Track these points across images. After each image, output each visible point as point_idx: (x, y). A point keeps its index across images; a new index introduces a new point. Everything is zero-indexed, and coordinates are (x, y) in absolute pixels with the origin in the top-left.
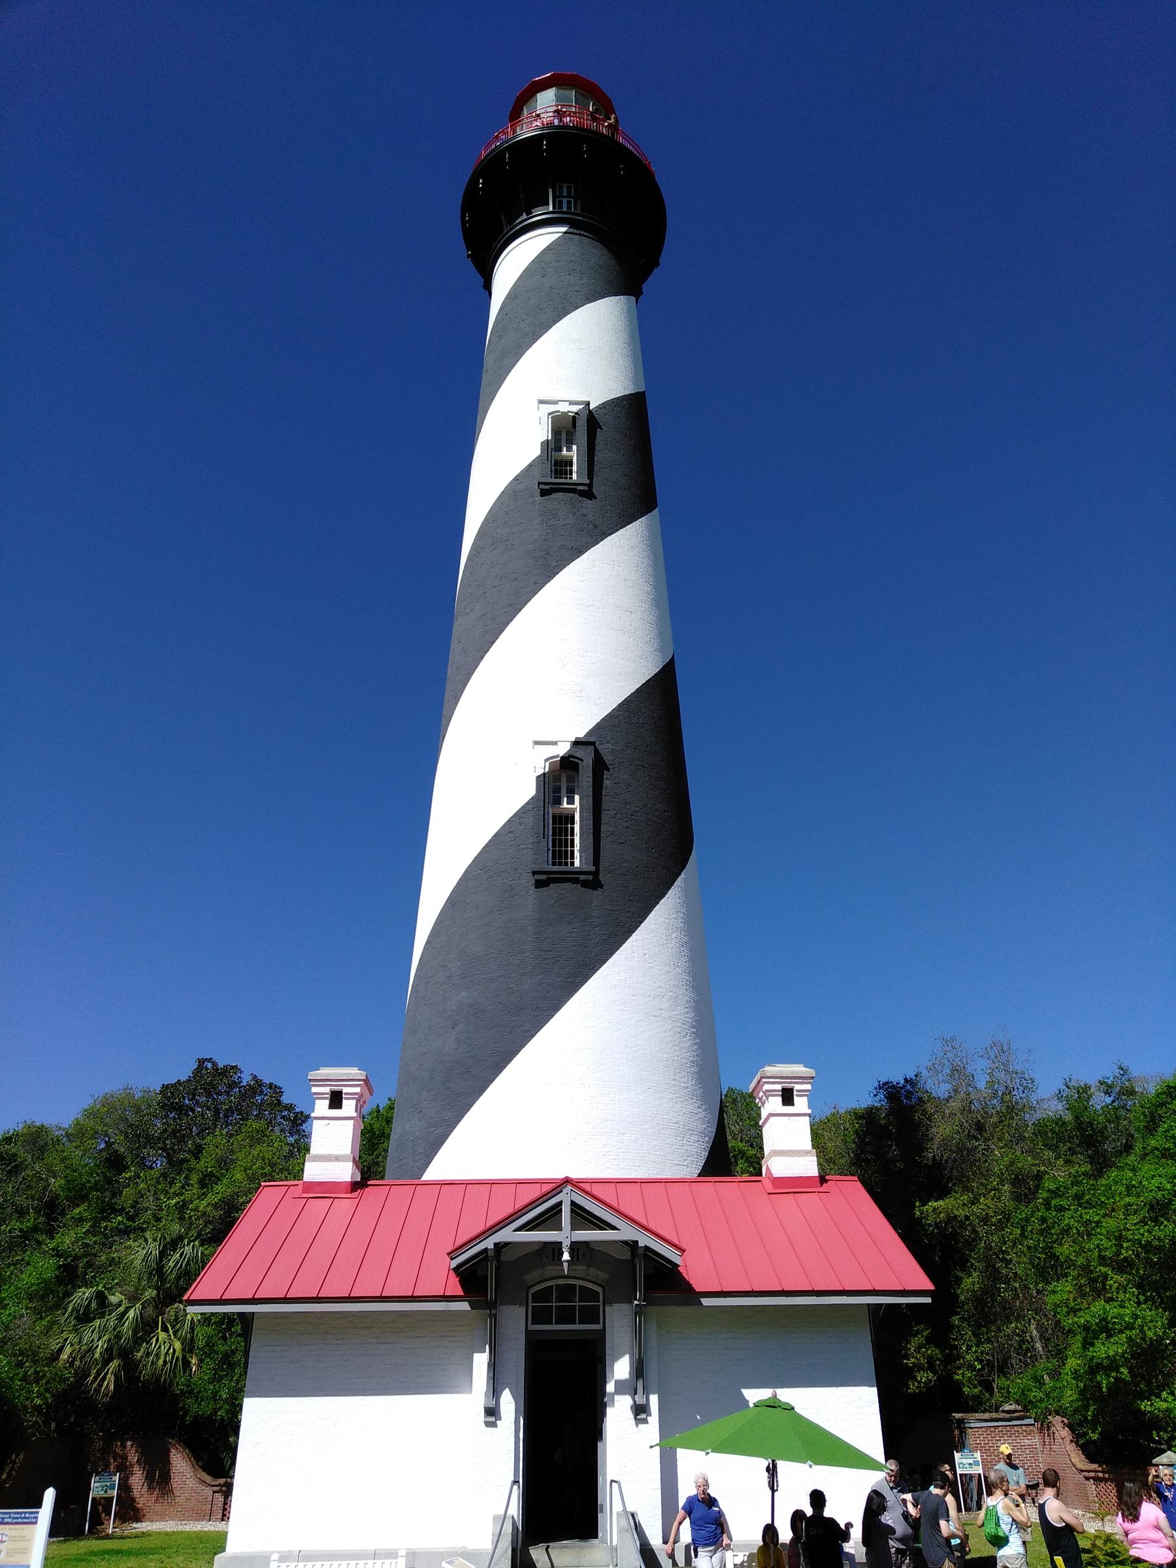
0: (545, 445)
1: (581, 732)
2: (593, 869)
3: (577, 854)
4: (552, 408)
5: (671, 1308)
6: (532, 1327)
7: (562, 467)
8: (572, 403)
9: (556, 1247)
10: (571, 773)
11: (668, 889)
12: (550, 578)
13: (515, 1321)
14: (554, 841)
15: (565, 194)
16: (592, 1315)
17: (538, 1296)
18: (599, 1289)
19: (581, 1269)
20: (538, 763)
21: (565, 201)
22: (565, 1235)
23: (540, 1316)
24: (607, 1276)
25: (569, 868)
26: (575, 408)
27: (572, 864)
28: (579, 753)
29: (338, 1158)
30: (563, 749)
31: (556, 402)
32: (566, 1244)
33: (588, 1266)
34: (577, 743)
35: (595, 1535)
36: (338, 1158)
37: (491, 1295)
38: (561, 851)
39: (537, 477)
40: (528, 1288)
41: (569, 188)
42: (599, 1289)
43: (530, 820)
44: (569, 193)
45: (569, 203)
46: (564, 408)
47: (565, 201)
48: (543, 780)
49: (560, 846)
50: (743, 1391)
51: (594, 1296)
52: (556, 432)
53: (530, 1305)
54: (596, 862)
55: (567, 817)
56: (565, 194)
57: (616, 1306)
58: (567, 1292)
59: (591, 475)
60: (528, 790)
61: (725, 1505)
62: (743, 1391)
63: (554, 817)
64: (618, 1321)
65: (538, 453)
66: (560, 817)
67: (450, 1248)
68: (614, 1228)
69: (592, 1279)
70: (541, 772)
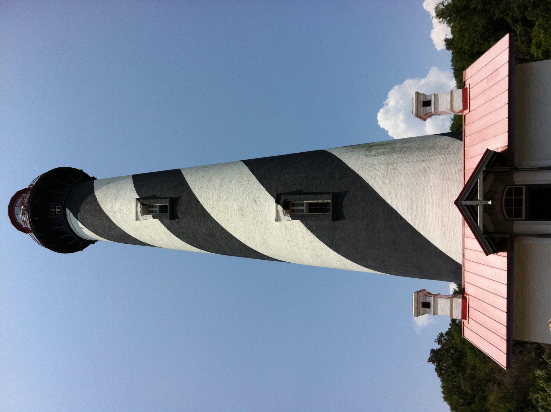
0: (154, 217)
1: (273, 200)
2: (331, 194)
3: (325, 202)
4: (139, 214)
7: (163, 209)
8: (137, 206)
9: (486, 208)
10: (291, 204)
11: (341, 160)
12: (209, 215)
13: (521, 226)
14: (320, 212)
16: (519, 190)
17: (510, 215)
18: (507, 187)
20: (286, 220)
21: (57, 210)
22: (479, 202)
23: (518, 214)
25: (331, 205)
26: (139, 205)
27: (329, 203)
28: (282, 200)
29: (451, 305)
30: (280, 208)
31: (137, 213)
32: (484, 203)
34: (278, 202)
36: (451, 305)
37: (507, 236)
38: (322, 208)
39: (167, 221)
40: (506, 220)
42: (507, 187)
45: (58, 208)
46: (139, 209)
47: (57, 210)
48: (293, 218)
49: (315, 206)
51: (510, 190)
52: (150, 212)
53: (514, 219)
54: (329, 193)
55: (309, 206)
58: (508, 203)
59: (166, 198)
60: (298, 224)
61: (26, 179)
63: (309, 212)
64: (523, 179)
65: (298, 221)
68: (477, 183)
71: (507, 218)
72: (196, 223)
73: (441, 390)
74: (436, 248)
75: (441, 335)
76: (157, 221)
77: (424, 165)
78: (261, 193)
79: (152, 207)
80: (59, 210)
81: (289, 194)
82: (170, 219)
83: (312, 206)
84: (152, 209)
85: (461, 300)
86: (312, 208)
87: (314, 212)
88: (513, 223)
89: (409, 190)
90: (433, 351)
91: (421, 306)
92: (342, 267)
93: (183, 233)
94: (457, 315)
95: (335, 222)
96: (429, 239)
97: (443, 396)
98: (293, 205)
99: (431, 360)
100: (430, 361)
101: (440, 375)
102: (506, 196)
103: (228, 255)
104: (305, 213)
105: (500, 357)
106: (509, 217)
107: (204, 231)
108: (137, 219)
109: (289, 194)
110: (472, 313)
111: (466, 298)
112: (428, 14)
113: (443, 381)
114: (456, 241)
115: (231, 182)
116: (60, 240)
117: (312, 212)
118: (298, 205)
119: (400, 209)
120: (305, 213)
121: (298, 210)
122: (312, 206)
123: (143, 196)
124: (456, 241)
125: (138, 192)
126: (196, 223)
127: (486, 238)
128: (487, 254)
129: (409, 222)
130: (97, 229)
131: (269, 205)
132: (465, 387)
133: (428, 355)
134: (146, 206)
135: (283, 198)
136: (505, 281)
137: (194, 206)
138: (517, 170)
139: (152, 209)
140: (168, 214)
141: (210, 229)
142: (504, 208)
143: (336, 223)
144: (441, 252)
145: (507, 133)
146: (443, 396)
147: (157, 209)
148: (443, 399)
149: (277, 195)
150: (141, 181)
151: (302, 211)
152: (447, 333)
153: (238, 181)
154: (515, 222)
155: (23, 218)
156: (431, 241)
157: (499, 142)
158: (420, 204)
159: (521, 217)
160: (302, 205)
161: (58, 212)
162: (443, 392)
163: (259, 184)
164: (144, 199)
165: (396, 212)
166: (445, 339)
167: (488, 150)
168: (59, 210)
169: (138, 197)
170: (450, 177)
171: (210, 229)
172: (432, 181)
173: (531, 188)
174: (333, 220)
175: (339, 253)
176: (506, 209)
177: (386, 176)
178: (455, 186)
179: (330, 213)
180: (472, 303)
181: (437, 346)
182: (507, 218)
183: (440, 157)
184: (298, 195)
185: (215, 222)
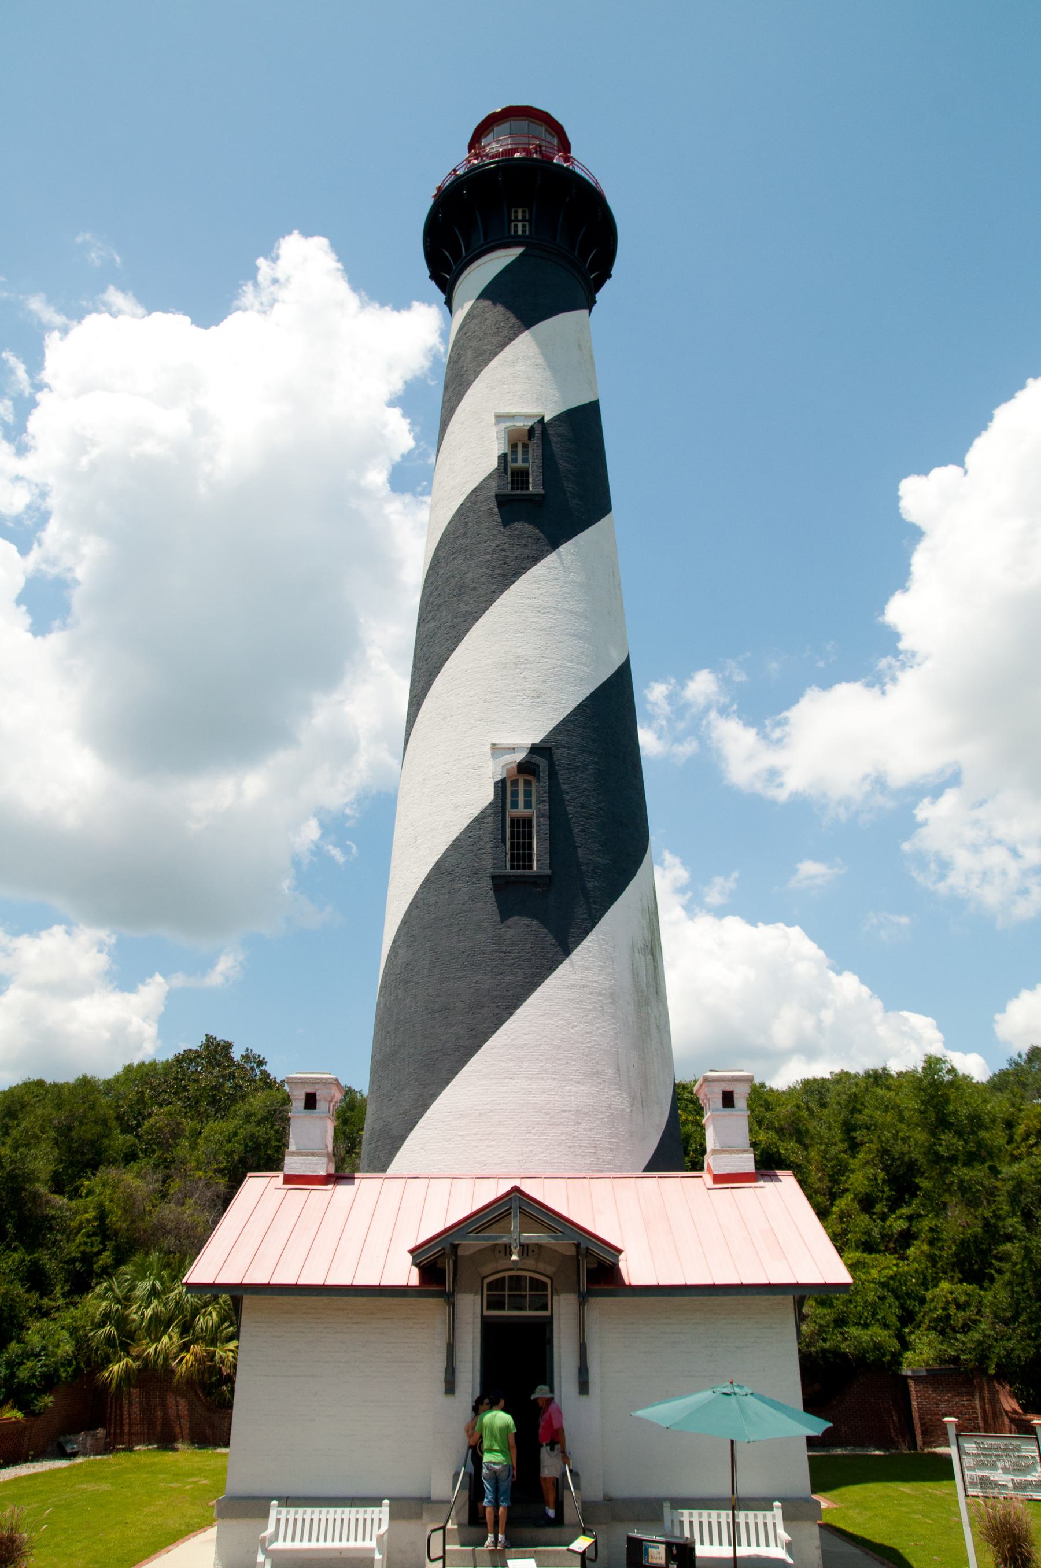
0: (503, 459)
1: (537, 741)
5: (599, 1299)
6: (487, 1313)
8: (527, 417)
12: (507, 586)
13: (471, 1308)
15: (520, 218)
17: (492, 1286)
18: (548, 1281)
19: (530, 1263)
21: (520, 225)
23: (494, 1303)
24: (554, 1269)
25: (527, 872)
30: (520, 756)
33: (537, 1260)
34: (534, 749)
35: (315, 1108)
38: (521, 855)
39: (493, 489)
40: (483, 1279)
41: (524, 212)
42: (548, 1281)
43: (489, 823)
44: (524, 217)
45: (524, 226)
47: (520, 225)
48: (501, 786)
49: (524, 832)
50: (831, 1425)
51: (544, 1286)
52: (514, 446)
55: (524, 820)
56: (520, 218)
57: (562, 1296)
58: (516, 1282)
60: (486, 795)
61: (591, 157)
62: (831, 1425)
63: (512, 821)
64: (563, 1309)
65: (492, 797)
66: (518, 821)
67: (442, 1386)
69: (542, 1270)
70: (499, 778)
71: (487, 1281)
72: (489, 557)
73: (213, 328)
74: (434, 1096)
75: (261, 1063)
76: (493, 464)
77: (610, 1072)
78: (555, 710)
79: (525, 452)
80: (520, 233)
81: (553, 774)
82: (497, 496)
83: (524, 827)
84: (520, 449)
85: (323, 1173)
86: (522, 827)
87: (512, 833)
88: (476, 1293)
89: (556, 1042)
90: (228, 1046)
91: (310, 1090)
92: (392, 891)
93: (466, 524)
94: (293, 1164)
95: (490, 880)
96: (453, 1083)
97: (135, 1065)
98: (527, 783)
99: (210, 1039)
100: (210, 1039)
101: (179, 1060)
102: (531, 1278)
103: (419, 626)
104: (511, 813)
105: (209, 1267)
106: (490, 1284)
107: (470, 575)
108: (500, 418)
109: (553, 774)
110: (298, 1196)
111: (326, 1184)
112: (954, 1049)
113: (168, 1066)
114: (449, 1140)
115: (580, 638)
116: (453, 234)
117: (512, 826)
118: (528, 794)
119: (515, 1024)
120: (511, 813)
121: (515, 794)
122: (524, 827)
123: (551, 431)
124: (449, 1140)
125: (559, 418)
126: (489, 557)
127: (443, 1249)
128: (411, 1252)
129: (488, 1043)
130: (475, 321)
131: (528, 731)
132: (158, 1118)
133: (221, 1036)
134: (526, 437)
135: (543, 763)
136: (357, 1282)
137: (527, 552)
138: (582, 1303)
139: (520, 449)
140: (508, 490)
141: (474, 589)
142: (507, 1274)
143: (487, 884)
144: (426, 1107)
145: (655, 1283)
146: (135, 1065)
147: (520, 464)
148: (127, 1063)
149: (550, 749)
150: (582, 425)
151: (515, 805)
152: (266, 1075)
153: (583, 653)
154: (478, 1298)
155: (495, 145)
156: (449, 1087)
157: (635, 1271)
158: (526, 1064)
159: (489, 1308)
160: (528, 805)
161: (516, 226)
162: (142, 1065)
163: (575, 705)
164: (544, 433)
165: (511, 1014)
166: (252, 1069)
167: (620, 1251)
168: (520, 233)
169: (546, 419)
170: (584, 1125)
171: (474, 589)
172: (574, 1089)
173: (548, 1322)
174: (494, 878)
175: (423, 886)
176: (504, 1278)
177: (587, 990)
178: (563, 1137)
179: (508, 871)
180: (319, 1195)
181: (237, 1054)
182: (487, 1281)
183: (626, 1104)
184: (550, 797)
185: (491, 602)
